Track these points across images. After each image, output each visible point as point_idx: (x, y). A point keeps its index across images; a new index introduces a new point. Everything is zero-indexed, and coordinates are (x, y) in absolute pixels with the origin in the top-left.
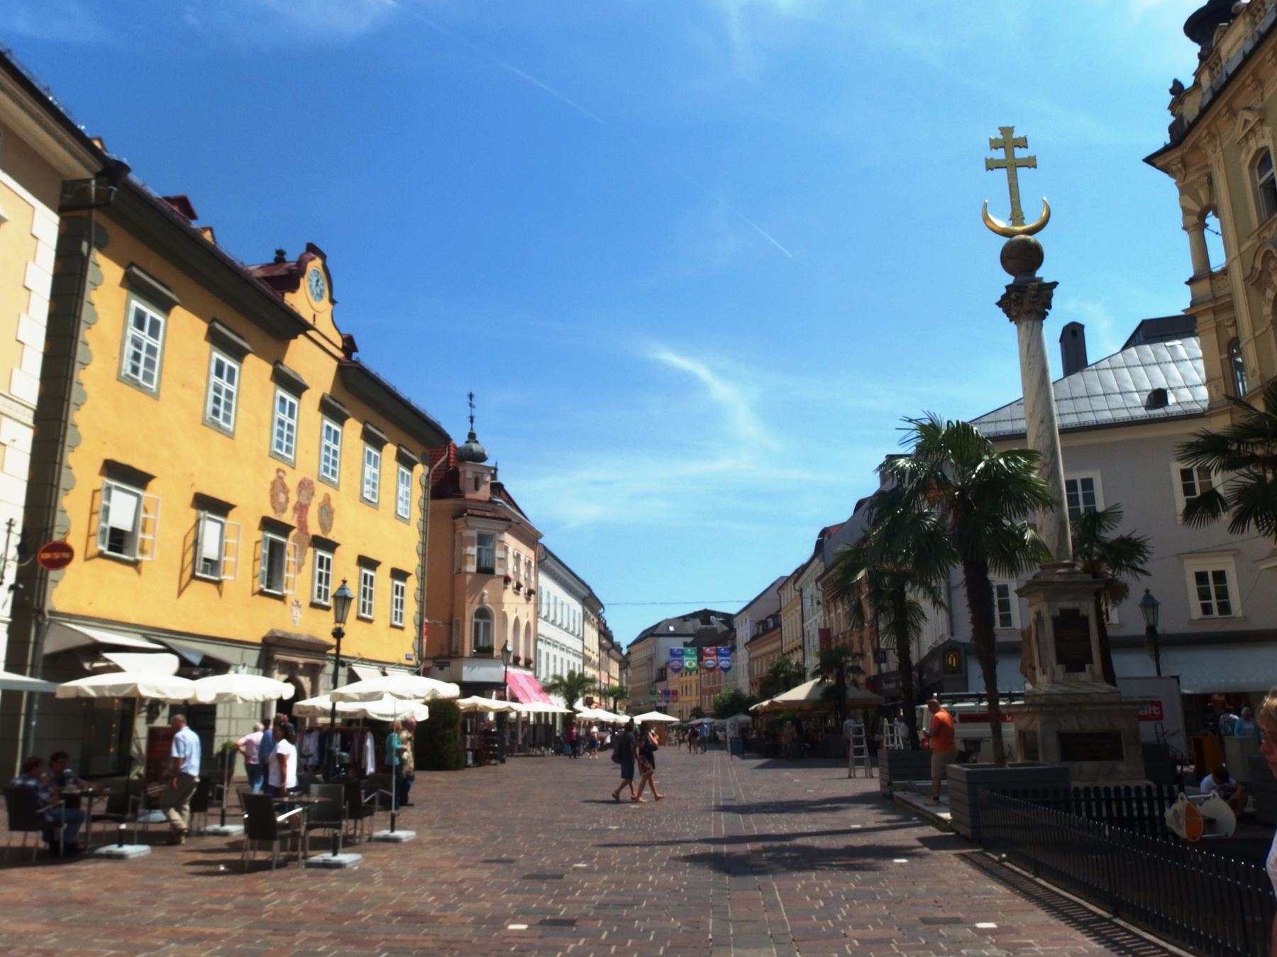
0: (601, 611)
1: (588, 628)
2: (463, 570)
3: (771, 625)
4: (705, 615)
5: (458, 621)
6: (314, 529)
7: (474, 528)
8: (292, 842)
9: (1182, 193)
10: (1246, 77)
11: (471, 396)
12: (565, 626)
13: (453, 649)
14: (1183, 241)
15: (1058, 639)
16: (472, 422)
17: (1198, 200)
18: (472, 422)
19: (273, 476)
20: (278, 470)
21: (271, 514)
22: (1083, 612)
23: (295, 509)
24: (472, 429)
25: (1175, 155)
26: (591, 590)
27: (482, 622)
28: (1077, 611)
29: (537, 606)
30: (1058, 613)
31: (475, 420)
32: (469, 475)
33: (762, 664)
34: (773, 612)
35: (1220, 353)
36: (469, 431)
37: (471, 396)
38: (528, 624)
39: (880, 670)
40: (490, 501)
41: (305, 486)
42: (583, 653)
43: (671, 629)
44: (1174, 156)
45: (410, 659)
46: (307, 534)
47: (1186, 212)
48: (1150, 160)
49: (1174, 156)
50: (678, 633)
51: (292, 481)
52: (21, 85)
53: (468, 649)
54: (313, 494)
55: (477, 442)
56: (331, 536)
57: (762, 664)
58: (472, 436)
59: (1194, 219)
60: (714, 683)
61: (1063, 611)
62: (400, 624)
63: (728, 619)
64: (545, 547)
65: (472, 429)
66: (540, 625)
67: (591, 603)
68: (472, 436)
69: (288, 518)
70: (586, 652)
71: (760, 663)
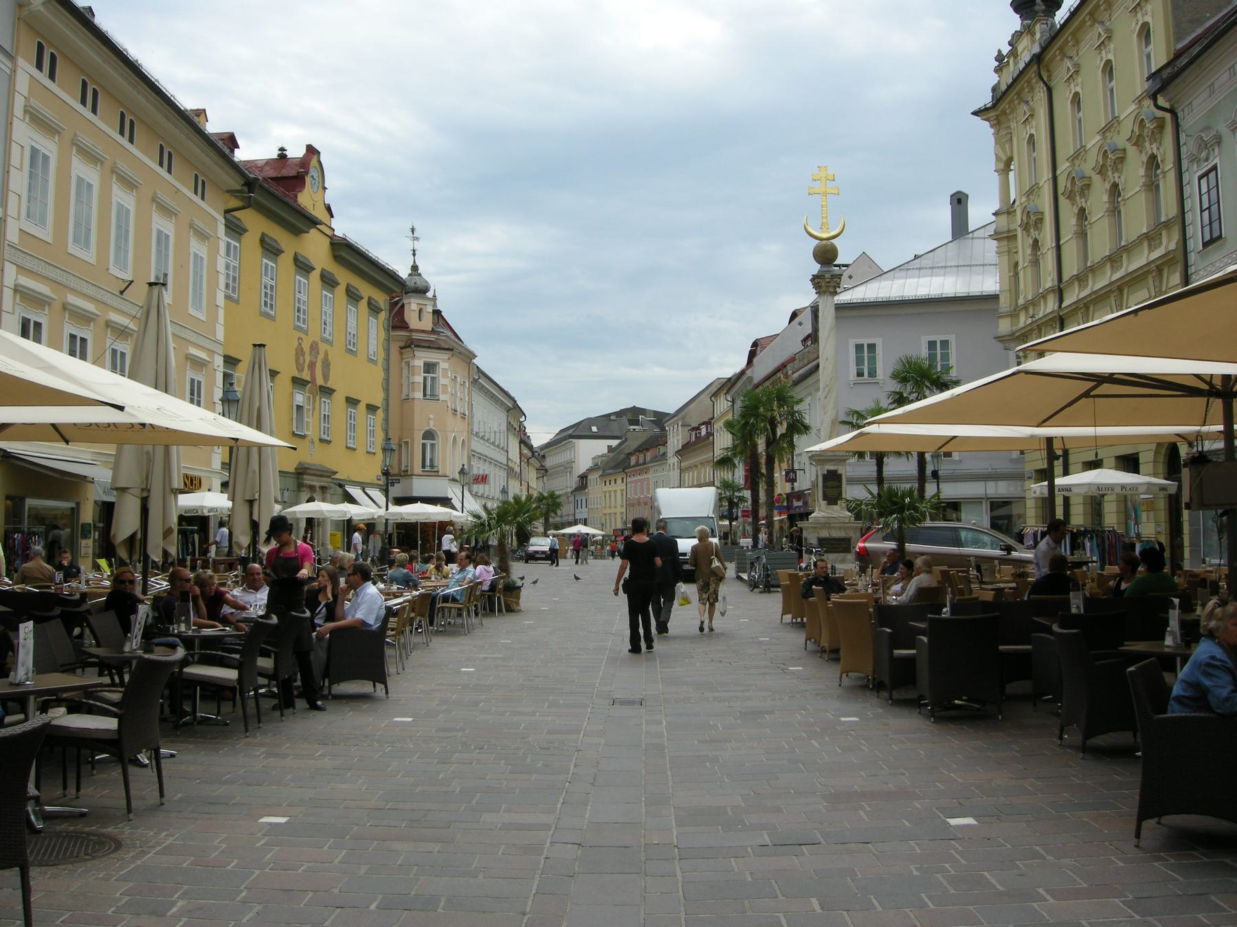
0: (522, 419)
1: (511, 438)
2: (411, 397)
3: (703, 432)
4: (633, 415)
5: (407, 443)
6: (320, 381)
7: (420, 358)
8: (239, 650)
9: (996, 143)
10: (1013, 94)
11: (413, 230)
12: (481, 435)
13: (403, 468)
14: (995, 179)
15: (824, 487)
16: (414, 255)
17: (1004, 150)
18: (414, 255)
19: (296, 344)
20: (299, 339)
21: (297, 375)
22: (839, 472)
23: (309, 366)
24: (414, 261)
25: (992, 114)
26: (515, 402)
27: (428, 442)
28: (835, 472)
29: (470, 424)
30: (826, 473)
31: (416, 252)
32: (414, 307)
33: (693, 478)
34: (706, 420)
35: (1009, 272)
36: (412, 263)
37: (413, 230)
38: (463, 441)
39: (793, 488)
40: (433, 332)
41: (314, 347)
42: (507, 465)
43: (594, 429)
44: (992, 115)
45: (380, 480)
46: (316, 385)
47: (998, 158)
48: (975, 113)
49: (992, 115)
50: (600, 434)
51: (306, 347)
52: (368, 282)
53: (418, 468)
54: (318, 353)
55: (420, 275)
56: (329, 385)
57: (693, 478)
58: (415, 268)
59: (1002, 166)
60: (642, 493)
61: (828, 471)
62: (328, 439)
63: (660, 419)
64: (477, 367)
65: (414, 261)
66: (473, 442)
67: (514, 410)
68: (415, 268)
69: (306, 375)
70: (510, 464)
71: (691, 475)
